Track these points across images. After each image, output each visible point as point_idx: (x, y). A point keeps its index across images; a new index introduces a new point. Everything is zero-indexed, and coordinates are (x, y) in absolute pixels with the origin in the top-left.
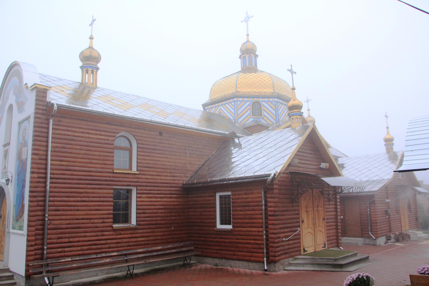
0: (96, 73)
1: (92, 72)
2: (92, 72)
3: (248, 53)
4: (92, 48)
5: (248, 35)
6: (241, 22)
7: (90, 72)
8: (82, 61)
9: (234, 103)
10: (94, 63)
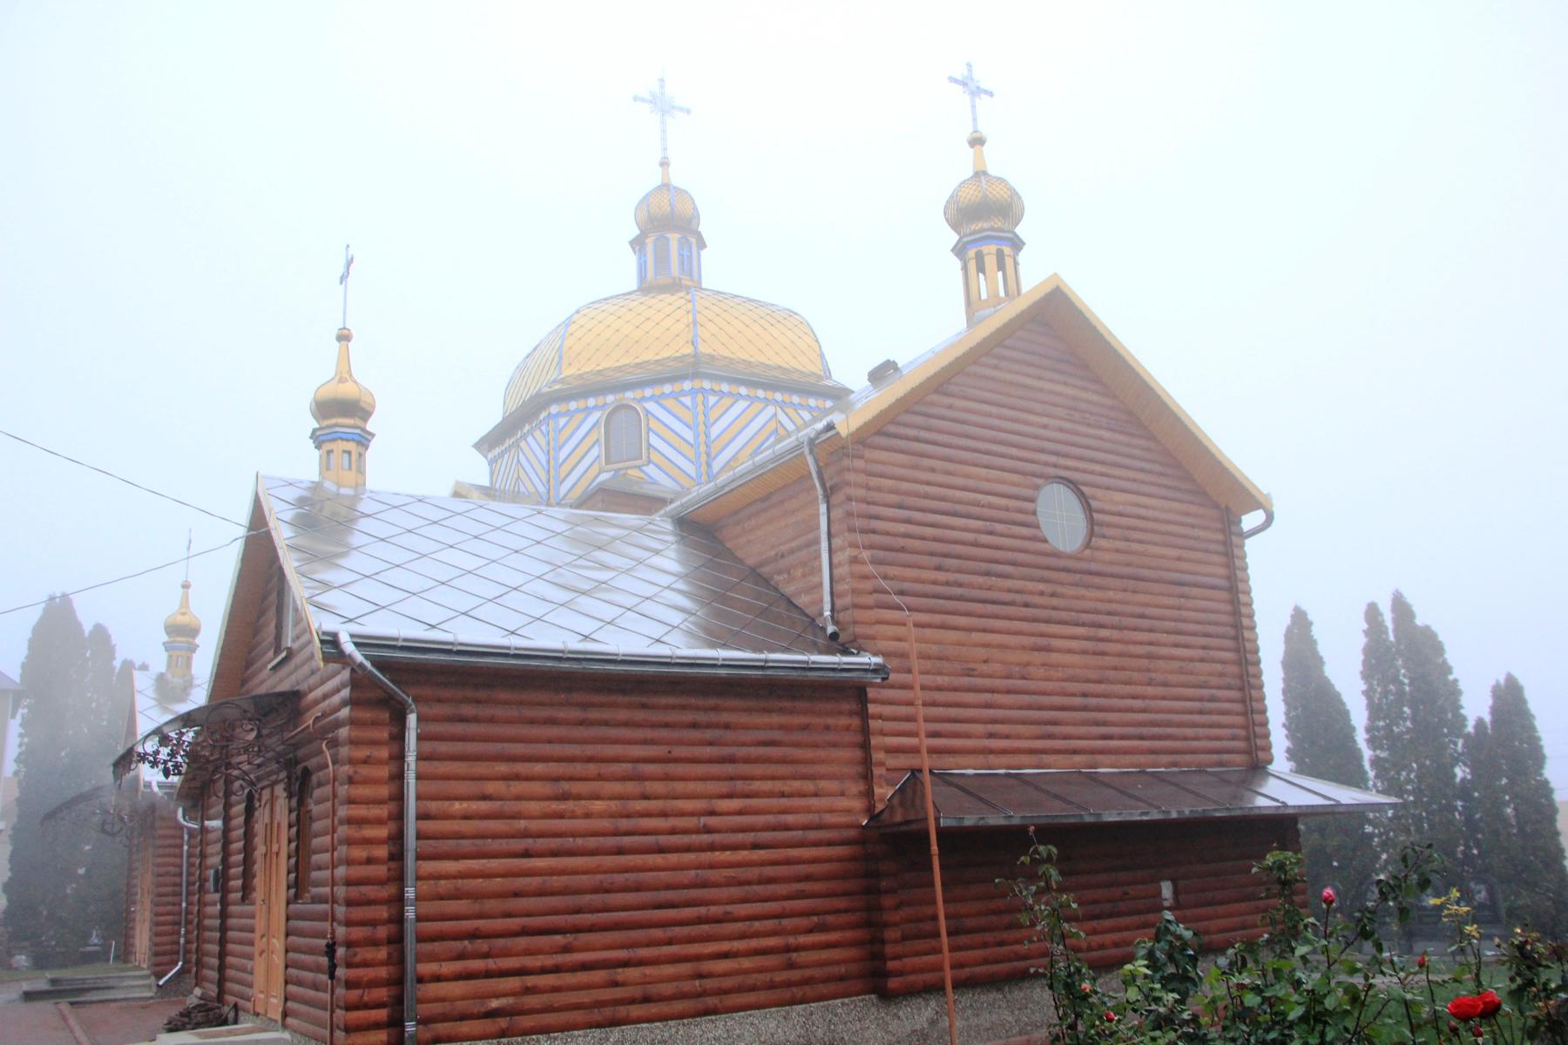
0: (1016, 264)
1: (1001, 266)
2: (1001, 266)
3: (668, 231)
4: (985, 173)
5: (664, 164)
6: (969, 65)
7: (991, 262)
8: (955, 225)
9: (693, 400)
10: (1005, 227)
